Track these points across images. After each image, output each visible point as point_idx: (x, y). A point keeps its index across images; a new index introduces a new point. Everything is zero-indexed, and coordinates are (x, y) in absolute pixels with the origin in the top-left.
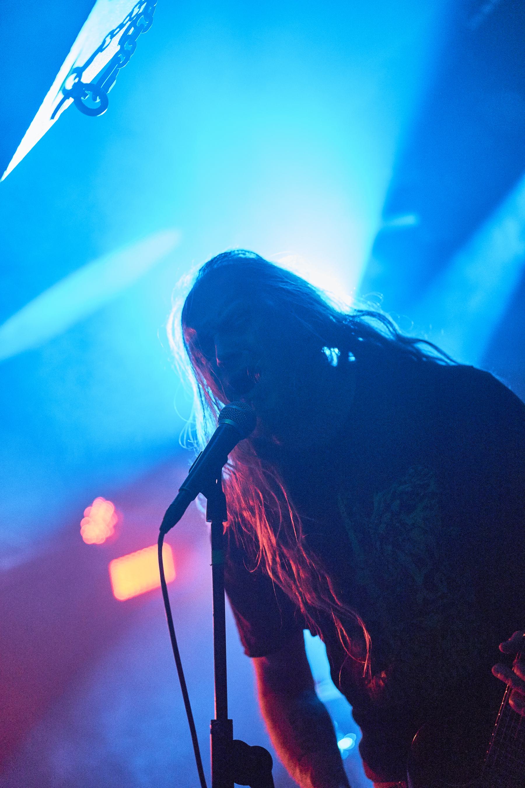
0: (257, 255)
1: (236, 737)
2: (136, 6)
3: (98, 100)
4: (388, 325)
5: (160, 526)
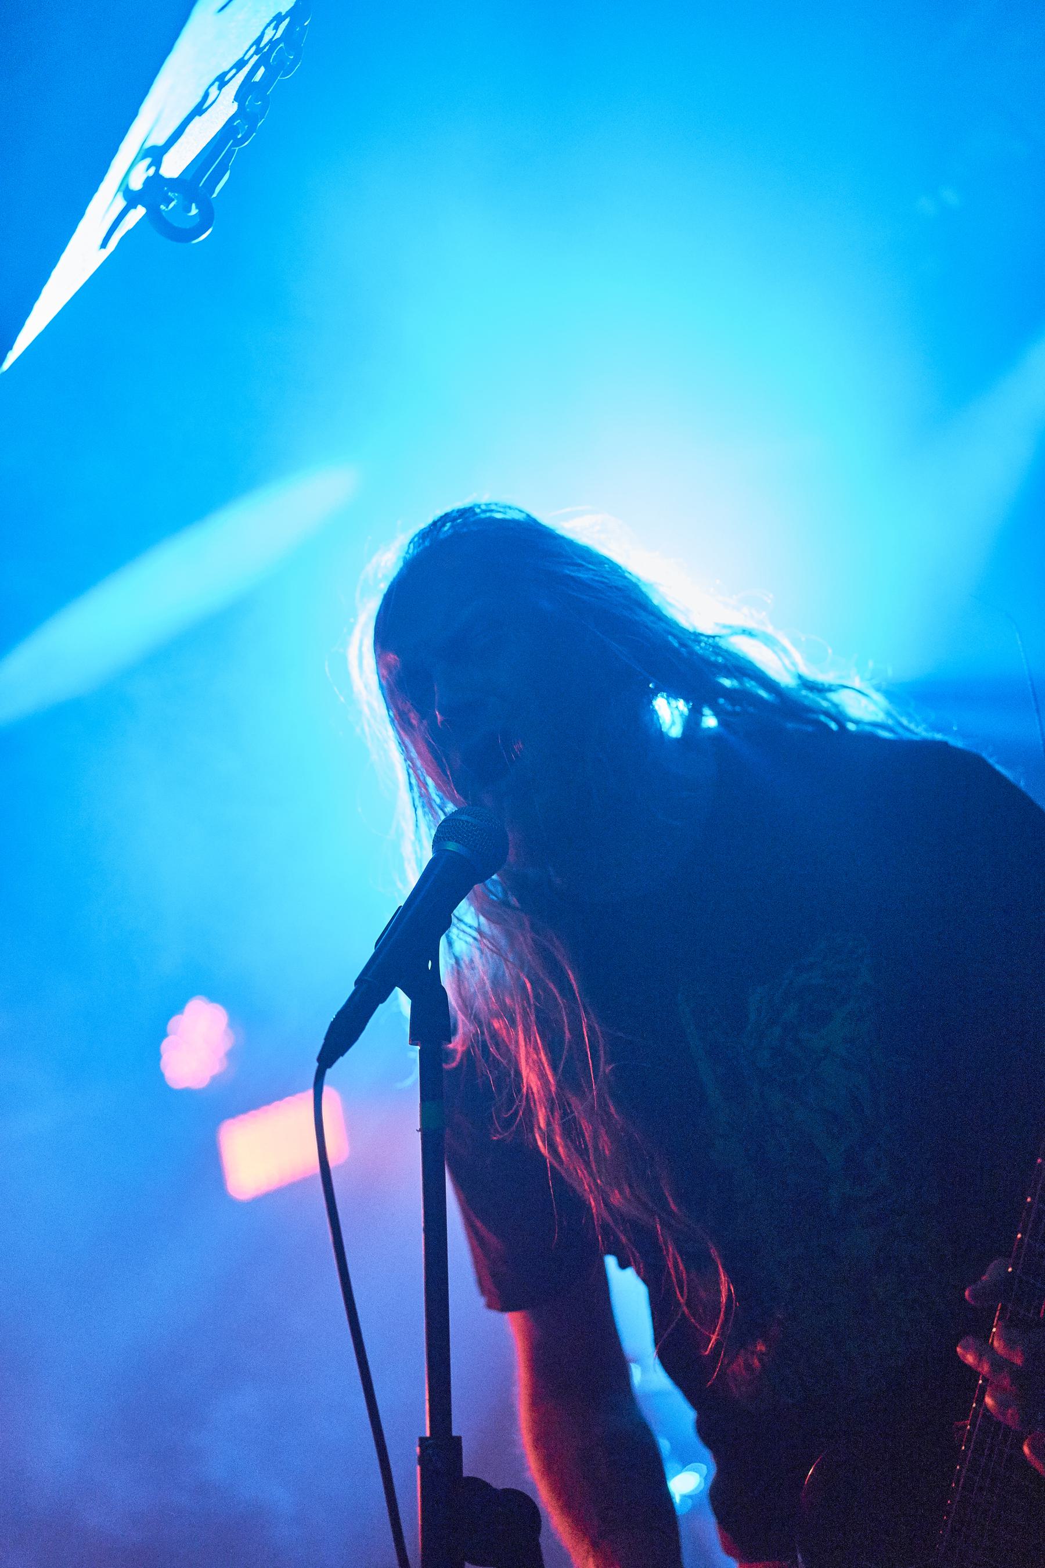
0: (528, 515)
1: (466, 1473)
2: (269, 25)
3: (194, 211)
4: (781, 653)
5: (317, 1054)
